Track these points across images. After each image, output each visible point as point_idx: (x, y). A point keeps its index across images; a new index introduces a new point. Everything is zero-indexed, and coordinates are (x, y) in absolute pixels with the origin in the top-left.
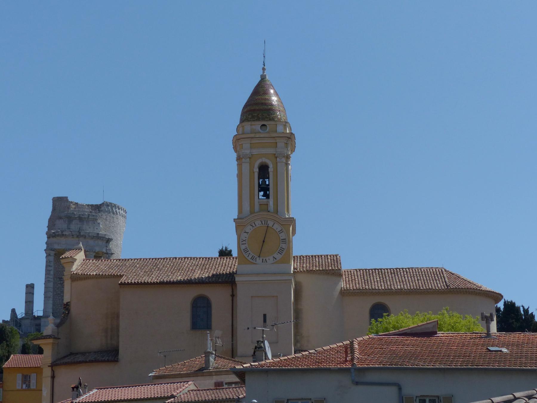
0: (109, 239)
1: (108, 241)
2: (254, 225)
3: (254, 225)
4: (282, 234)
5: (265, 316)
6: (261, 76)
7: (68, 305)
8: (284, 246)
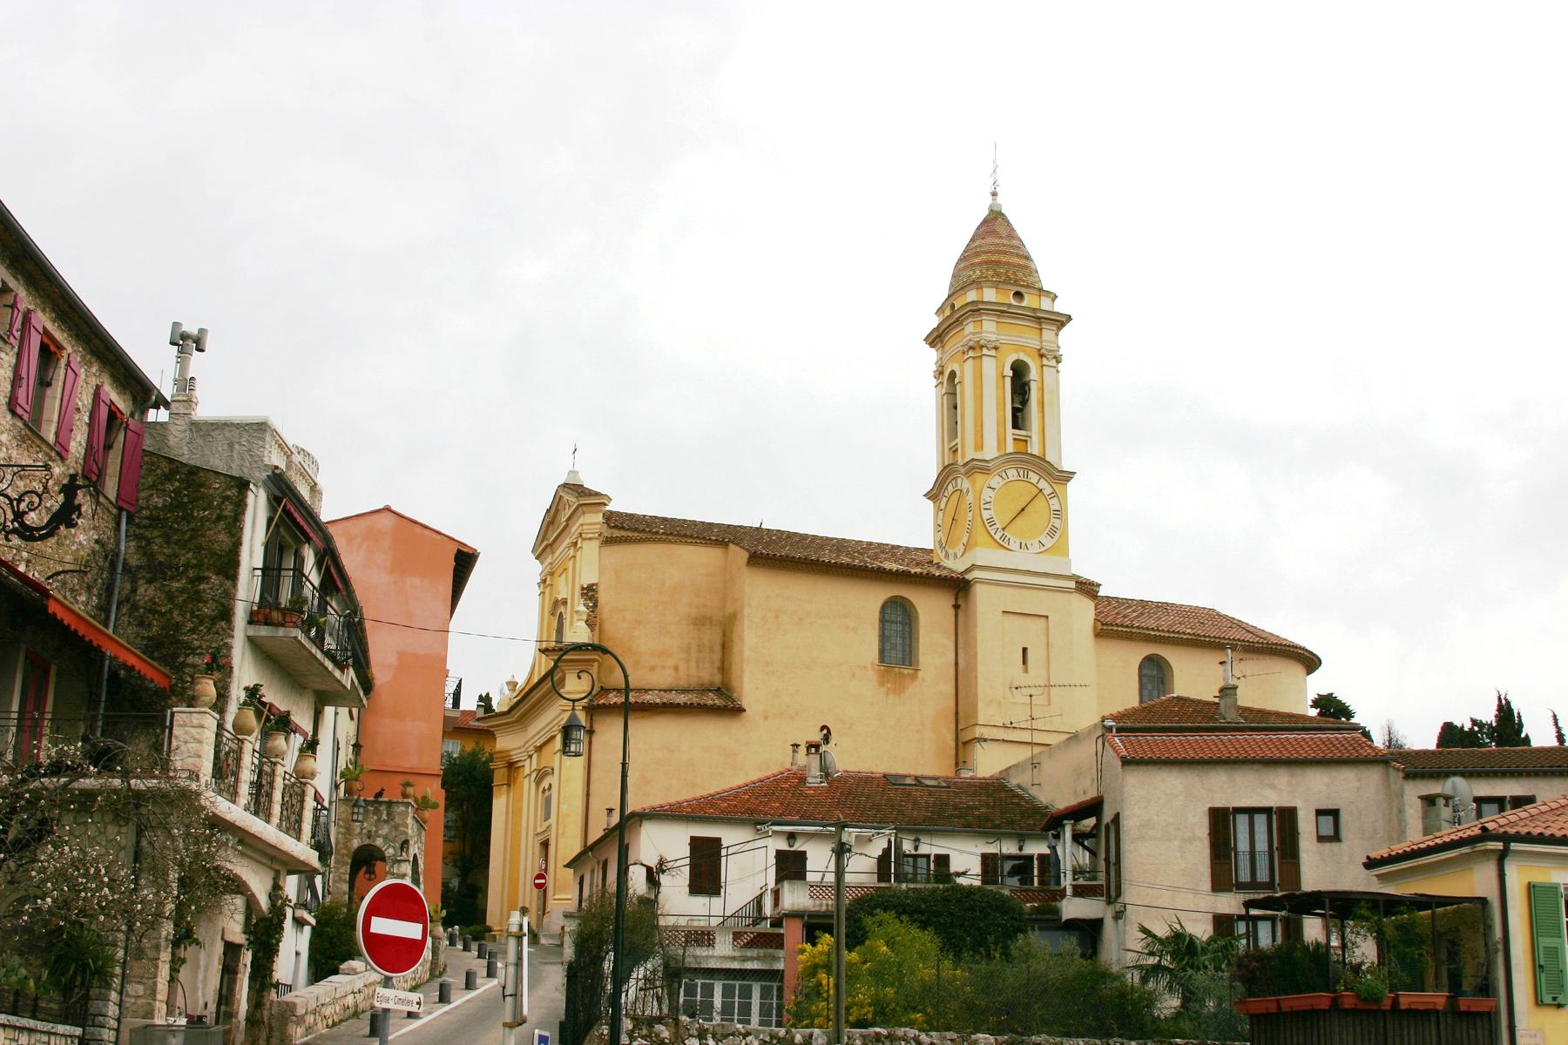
5: (1025, 650)
8: (1057, 523)
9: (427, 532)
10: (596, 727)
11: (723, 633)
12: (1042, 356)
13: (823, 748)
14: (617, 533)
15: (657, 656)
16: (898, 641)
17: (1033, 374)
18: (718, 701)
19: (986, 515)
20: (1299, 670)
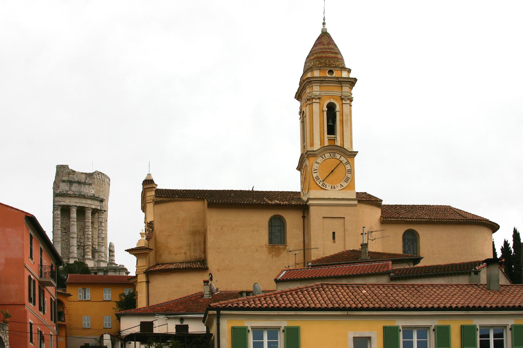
0: (102, 199)
1: (102, 201)
2: (323, 156)
3: (323, 156)
5: (334, 233)
7: (152, 224)
8: (349, 176)
9: (13, 210)
10: (150, 280)
11: (200, 235)
12: (342, 99)
13: (210, 282)
14: (159, 199)
16: (277, 235)
17: (338, 108)
18: (199, 265)
19: (315, 175)
20: (486, 231)
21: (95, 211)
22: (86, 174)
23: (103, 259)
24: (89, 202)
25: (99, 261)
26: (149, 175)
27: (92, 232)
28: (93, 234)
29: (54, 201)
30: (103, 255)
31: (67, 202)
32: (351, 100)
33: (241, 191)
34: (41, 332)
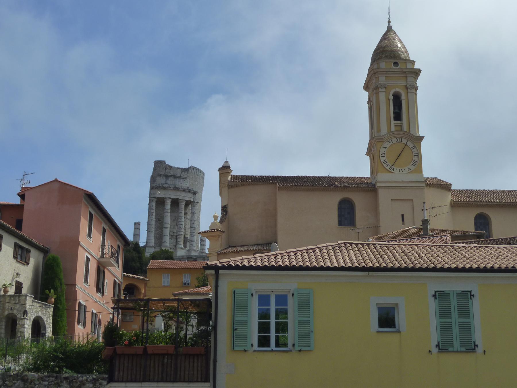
1: (195, 193)
2: (390, 141)
3: (390, 141)
4: (415, 150)
5: (403, 215)
6: (388, 27)
8: (416, 159)
11: (271, 216)
15: (249, 227)
17: (403, 97)
19: (382, 159)
21: (188, 203)
22: (182, 169)
23: (195, 248)
24: (183, 194)
25: (190, 250)
26: (227, 162)
27: (185, 222)
28: (185, 224)
29: (151, 194)
30: (195, 244)
31: (160, 194)
32: (416, 89)
33: (314, 177)
34: (96, 315)
